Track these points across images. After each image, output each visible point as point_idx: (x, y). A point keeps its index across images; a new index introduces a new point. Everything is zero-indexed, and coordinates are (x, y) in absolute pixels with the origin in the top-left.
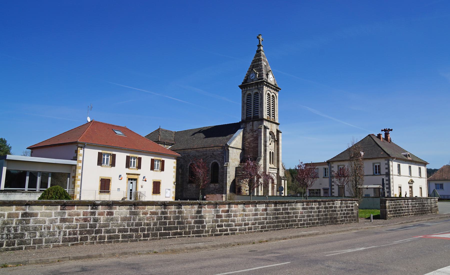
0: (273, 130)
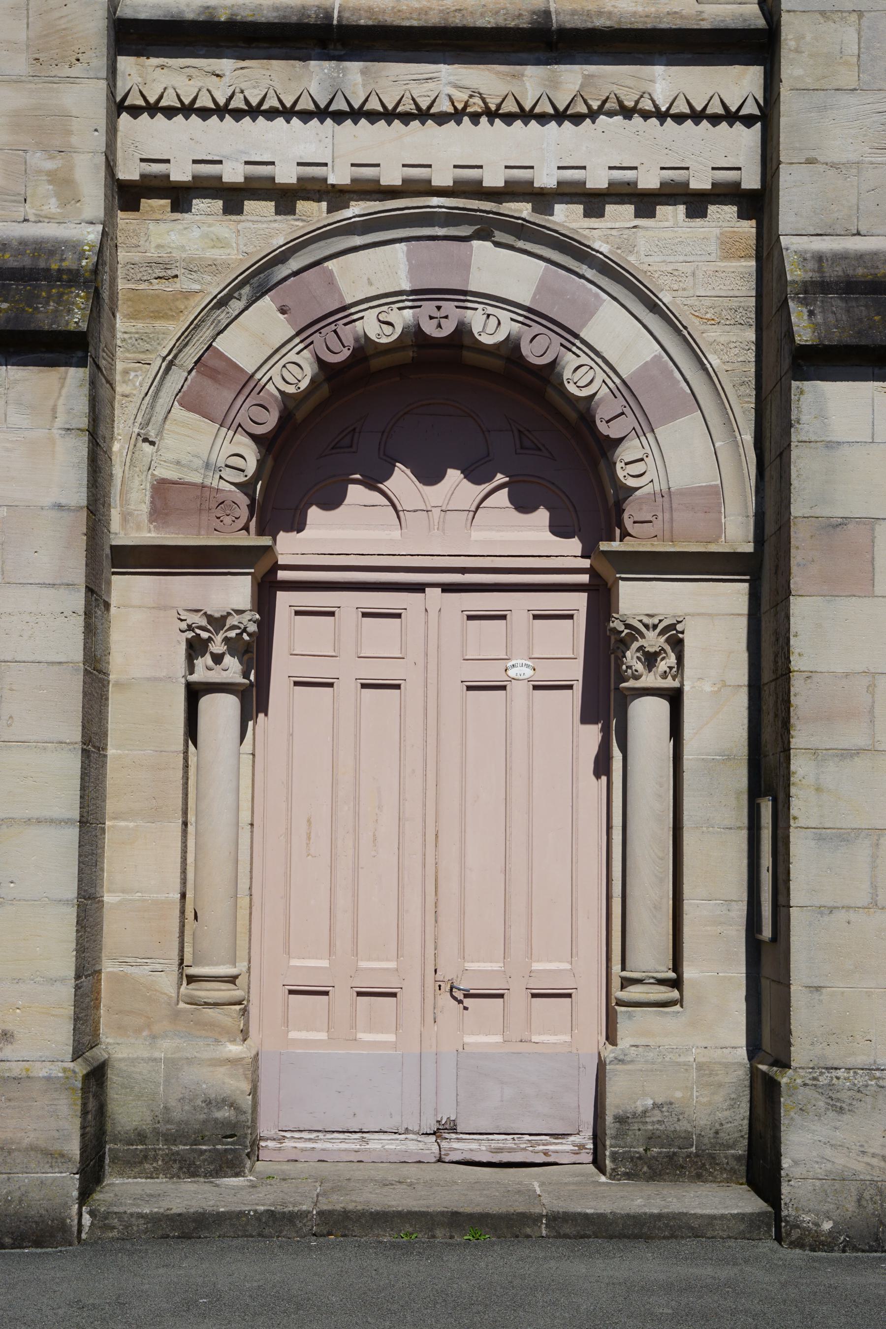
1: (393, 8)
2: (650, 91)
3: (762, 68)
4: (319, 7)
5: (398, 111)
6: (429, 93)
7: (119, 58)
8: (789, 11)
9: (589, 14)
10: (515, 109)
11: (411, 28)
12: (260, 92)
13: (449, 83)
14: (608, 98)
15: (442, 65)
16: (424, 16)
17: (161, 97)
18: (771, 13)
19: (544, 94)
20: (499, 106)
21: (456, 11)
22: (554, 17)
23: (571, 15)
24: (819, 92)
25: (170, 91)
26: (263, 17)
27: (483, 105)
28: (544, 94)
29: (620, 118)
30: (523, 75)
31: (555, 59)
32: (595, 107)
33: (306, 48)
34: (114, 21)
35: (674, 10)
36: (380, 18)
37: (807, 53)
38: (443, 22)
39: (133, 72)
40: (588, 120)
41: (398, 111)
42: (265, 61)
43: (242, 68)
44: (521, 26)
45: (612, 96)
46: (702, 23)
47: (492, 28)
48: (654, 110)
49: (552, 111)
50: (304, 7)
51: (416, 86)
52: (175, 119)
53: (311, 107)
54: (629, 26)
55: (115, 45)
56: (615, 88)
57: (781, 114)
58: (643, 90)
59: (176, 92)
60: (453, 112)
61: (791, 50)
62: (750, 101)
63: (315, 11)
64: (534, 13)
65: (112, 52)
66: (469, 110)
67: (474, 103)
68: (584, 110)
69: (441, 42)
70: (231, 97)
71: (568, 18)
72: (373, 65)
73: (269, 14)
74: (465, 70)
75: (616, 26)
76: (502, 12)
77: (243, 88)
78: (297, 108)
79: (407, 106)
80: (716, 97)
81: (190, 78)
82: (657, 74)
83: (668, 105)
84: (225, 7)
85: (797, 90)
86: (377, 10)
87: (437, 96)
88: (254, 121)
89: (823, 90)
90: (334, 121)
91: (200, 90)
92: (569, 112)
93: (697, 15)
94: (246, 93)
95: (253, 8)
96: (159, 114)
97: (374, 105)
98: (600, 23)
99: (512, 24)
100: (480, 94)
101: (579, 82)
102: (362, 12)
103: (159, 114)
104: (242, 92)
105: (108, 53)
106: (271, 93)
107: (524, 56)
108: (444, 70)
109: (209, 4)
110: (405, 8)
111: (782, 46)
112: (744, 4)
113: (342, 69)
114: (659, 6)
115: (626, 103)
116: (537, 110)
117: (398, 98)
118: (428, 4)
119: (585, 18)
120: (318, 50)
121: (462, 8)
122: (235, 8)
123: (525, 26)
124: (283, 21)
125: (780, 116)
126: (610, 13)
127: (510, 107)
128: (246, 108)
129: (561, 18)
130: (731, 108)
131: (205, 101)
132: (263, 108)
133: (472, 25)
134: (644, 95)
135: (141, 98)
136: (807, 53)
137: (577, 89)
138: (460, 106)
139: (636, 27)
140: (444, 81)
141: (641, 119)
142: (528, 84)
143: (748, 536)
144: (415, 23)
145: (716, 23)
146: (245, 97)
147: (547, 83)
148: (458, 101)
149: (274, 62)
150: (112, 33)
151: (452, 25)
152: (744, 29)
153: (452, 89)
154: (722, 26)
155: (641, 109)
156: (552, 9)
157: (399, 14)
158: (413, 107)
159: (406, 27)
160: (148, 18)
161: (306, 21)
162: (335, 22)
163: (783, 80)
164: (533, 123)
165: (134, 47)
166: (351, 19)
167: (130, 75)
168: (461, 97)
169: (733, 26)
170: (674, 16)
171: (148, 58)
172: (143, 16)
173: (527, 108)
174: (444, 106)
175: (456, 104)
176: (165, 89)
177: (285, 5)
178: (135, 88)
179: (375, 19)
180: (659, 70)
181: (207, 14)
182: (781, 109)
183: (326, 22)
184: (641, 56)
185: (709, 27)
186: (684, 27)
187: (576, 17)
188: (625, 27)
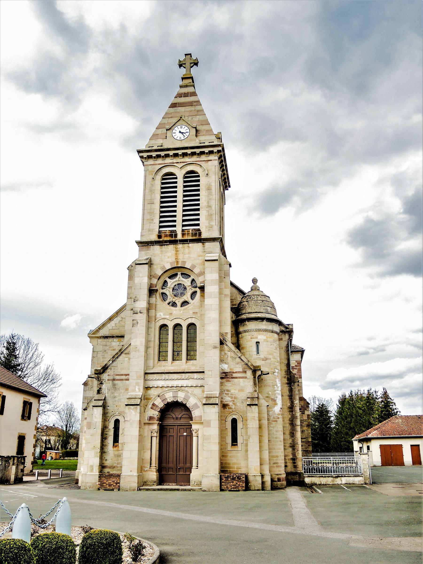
0: (184, 262)
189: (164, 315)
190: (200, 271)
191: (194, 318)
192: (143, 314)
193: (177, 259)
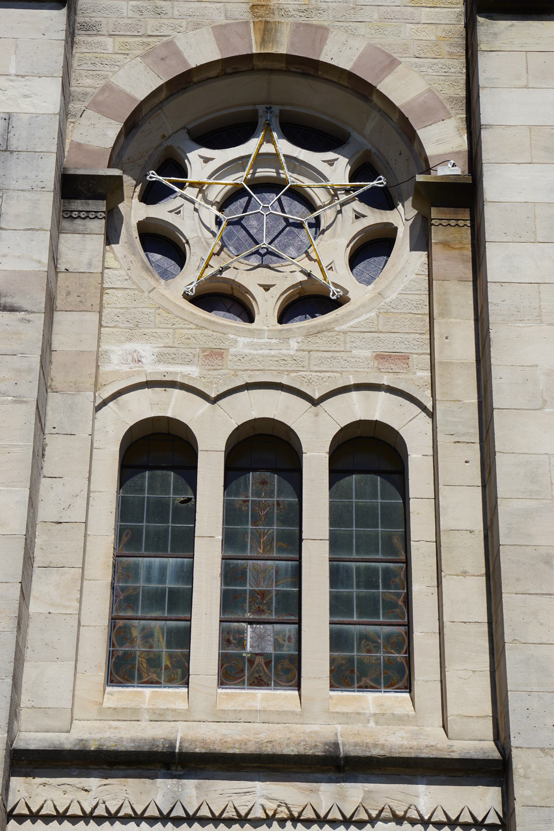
1: (221, 740)
2: (415, 804)
3: (500, 788)
4: (165, 739)
5: (223, 817)
6: (247, 803)
7: (12, 778)
8: (517, 748)
9: (367, 745)
10: (313, 816)
11: (234, 755)
12: (117, 803)
13: (263, 796)
14: (383, 809)
15: (257, 782)
16: (244, 746)
17: (42, 807)
18: (503, 749)
19: (335, 804)
20: (300, 814)
21: (268, 742)
22: (341, 747)
23: (354, 746)
24: (545, 808)
25: (49, 803)
26: (123, 746)
27: (288, 813)
28: (335, 805)
29: (393, 824)
30: (318, 790)
31: (343, 779)
32: (374, 816)
33: (155, 770)
34: (11, 751)
35: (431, 744)
36: (211, 747)
37: (533, 779)
38: (258, 750)
39: (22, 789)
40: (369, 825)
41: (223, 817)
42: (123, 779)
43: (105, 785)
44: (317, 754)
45: (387, 807)
46: (452, 754)
47: (295, 755)
48: (419, 818)
49: (340, 818)
50: (154, 739)
51: (237, 797)
52: (51, 824)
53: (157, 814)
54: (398, 755)
55: (10, 769)
56: (388, 801)
57: (517, 824)
58: (410, 803)
59: (54, 803)
60: (265, 817)
61: (521, 776)
62: (492, 813)
63: (163, 742)
64: (326, 744)
65: (7, 774)
66: (277, 816)
67: (282, 811)
68: (365, 817)
69: (256, 765)
70: (95, 807)
71: (352, 748)
72: (205, 782)
73: (128, 745)
74: (274, 786)
75: (388, 755)
76: (302, 743)
77: (105, 800)
78: (146, 815)
79: (230, 813)
80: (466, 810)
81: (65, 793)
82: (420, 791)
83: (429, 815)
84: (95, 740)
85: (528, 806)
86: (209, 741)
87: (253, 806)
88: (112, 825)
89: (548, 807)
90: (174, 825)
91: (72, 802)
92: (354, 819)
93: (448, 748)
94: (107, 804)
95: (116, 740)
96: (39, 820)
97: (205, 812)
98: (375, 752)
99: (310, 752)
100: (286, 804)
101: (361, 796)
102: (197, 743)
103: (39, 820)
104: (104, 803)
105: (4, 775)
106: (126, 803)
107: (319, 775)
108: (258, 786)
109: (82, 738)
110: (230, 740)
111: (514, 773)
112: (483, 740)
113: (182, 785)
114: (420, 741)
115: (398, 813)
116: (330, 817)
117: (224, 807)
118: (247, 737)
119: (364, 748)
120: (163, 771)
121: (272, 740)
122: (102, 741)
123: (320, 754)
124: (138, 750)
125: (516, 826)
126: (383, 745)
127: (309, 815)
128: (107, 815)
129: (347, 748)
130: (478, 818)
131: (75, 810)
132: (119, 815)
133: (279, 753)
134: (411, 807)
135: (26, 808)
136: (533, 779)
137: (360, 801)
138: (270, 813)
139: (403, 756)
140: (258, 794)
141: (409, 825)
142: (322, 797)
143: (444, 162)
144: (237, 751)
145: (463, 754)
146: (106, 807)
147: (337, 796)
148: (269, 810)
149: (130, 780)
150: (8, 760)
151: (265, 753)
152: (484, 760)
153: (264, 800)
154: (468, 756)
155: (409, 817)
156: (340, 742)
157: (225, 744)
158: (235, 814)
159: (230, 754)
160: (36, 749)
161: (155, 749)
162: (177, 750)
163: (516, 798)
164: (327, 826)
165: (24, 770)
166: (189, 748)
167: (19, 791)
168: (271, 807)
169: (475, 757)
170: (431, 748)
171: (34, 778)
172: (32, 747)
173: (322, 815)
174: (258, 813)
175: (267, 812)
176: (45, 801)
177: (140, 738)
178: (23, 802)
179: (207, 748)
180: (421, 788)
181: (81, 745)
182: (517, 821)
183: (170, 750)
184: (408, 777)
185: (458, 757)
186: (439, 756)
187: (358, 748)
188: (395, 756)
189: (161, 358)
190: (430, 91)
191: (382, 395)
192: (22, 320)
193: (261, 11)
